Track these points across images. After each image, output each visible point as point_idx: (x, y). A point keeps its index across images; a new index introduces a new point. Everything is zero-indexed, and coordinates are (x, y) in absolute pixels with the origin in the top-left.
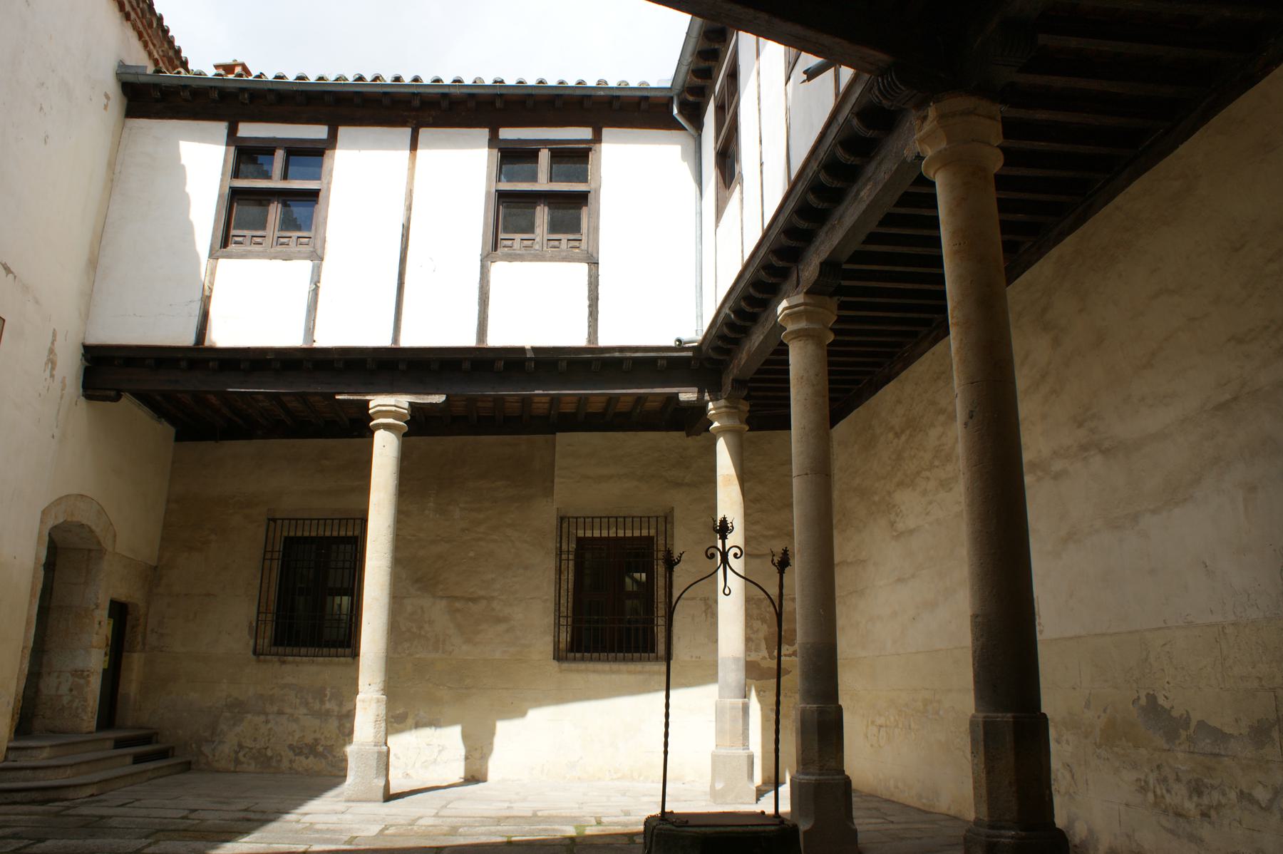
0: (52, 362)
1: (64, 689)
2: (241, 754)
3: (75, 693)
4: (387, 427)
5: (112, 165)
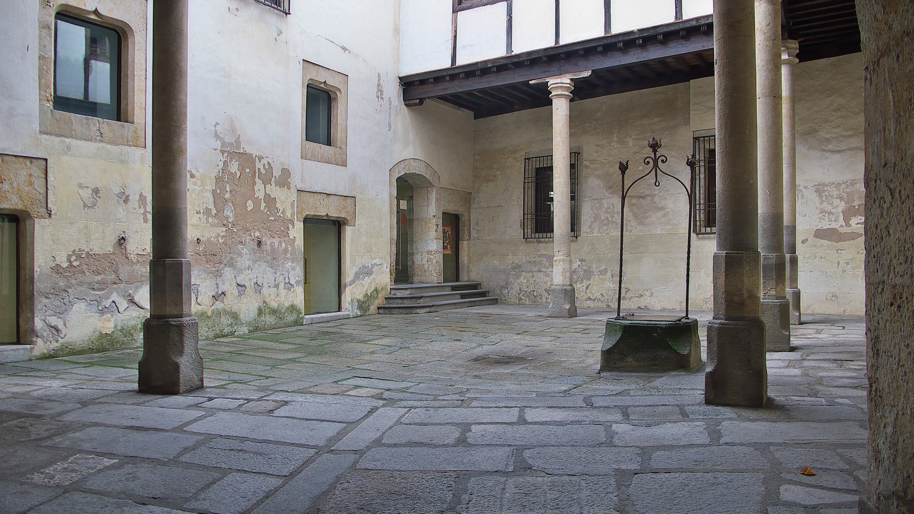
0: (380, 91)
1: (425, 261)
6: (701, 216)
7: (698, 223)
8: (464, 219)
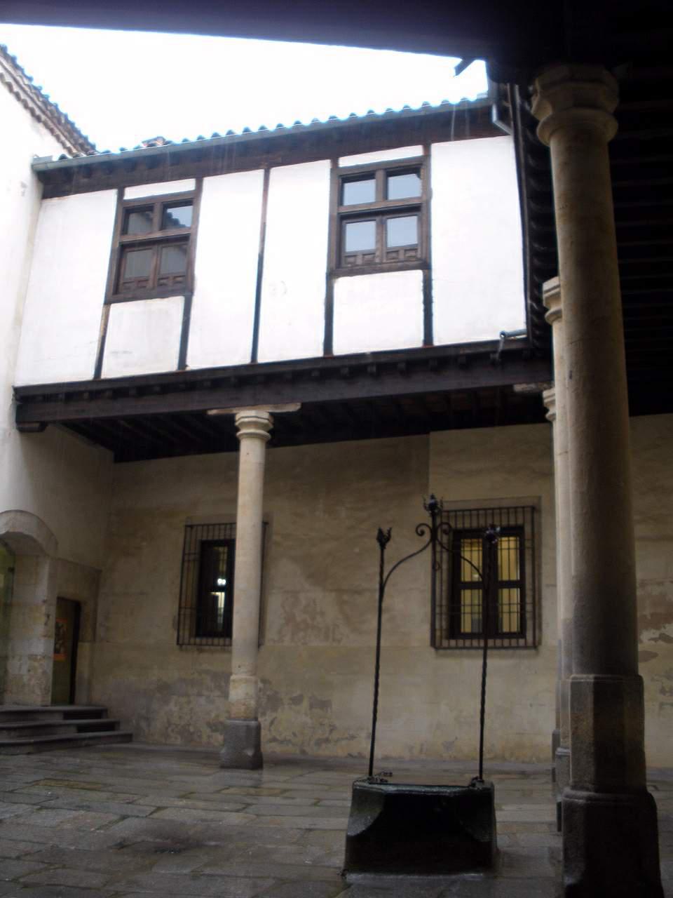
2: (170, 729)
3: (32, 673)
5: (31, 239)
6: (442, 623)
7: (438, 633)
8: (87, 609)
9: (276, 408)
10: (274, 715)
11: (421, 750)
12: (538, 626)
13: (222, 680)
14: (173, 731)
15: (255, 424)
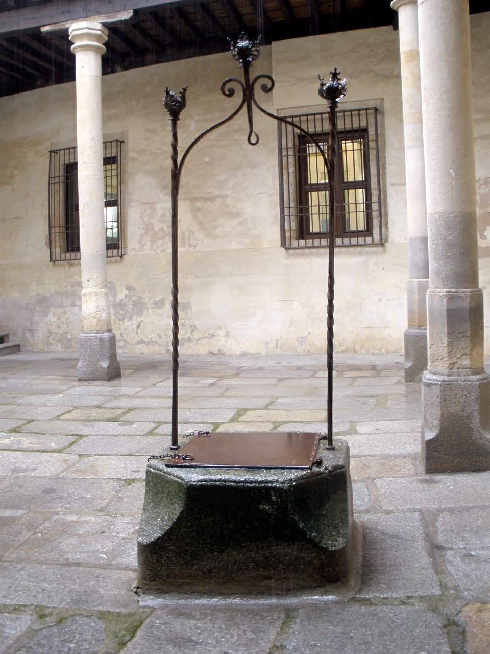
2: (51, 338)
4: (84, 48)
6: (292, 224)
7: (288, 234)
9: (109, 17)
10: (140, 319)
11: (277, 346)
12: (384, 224)
13: (73, 294)
14: (53, 339)
15: (89, 36)
